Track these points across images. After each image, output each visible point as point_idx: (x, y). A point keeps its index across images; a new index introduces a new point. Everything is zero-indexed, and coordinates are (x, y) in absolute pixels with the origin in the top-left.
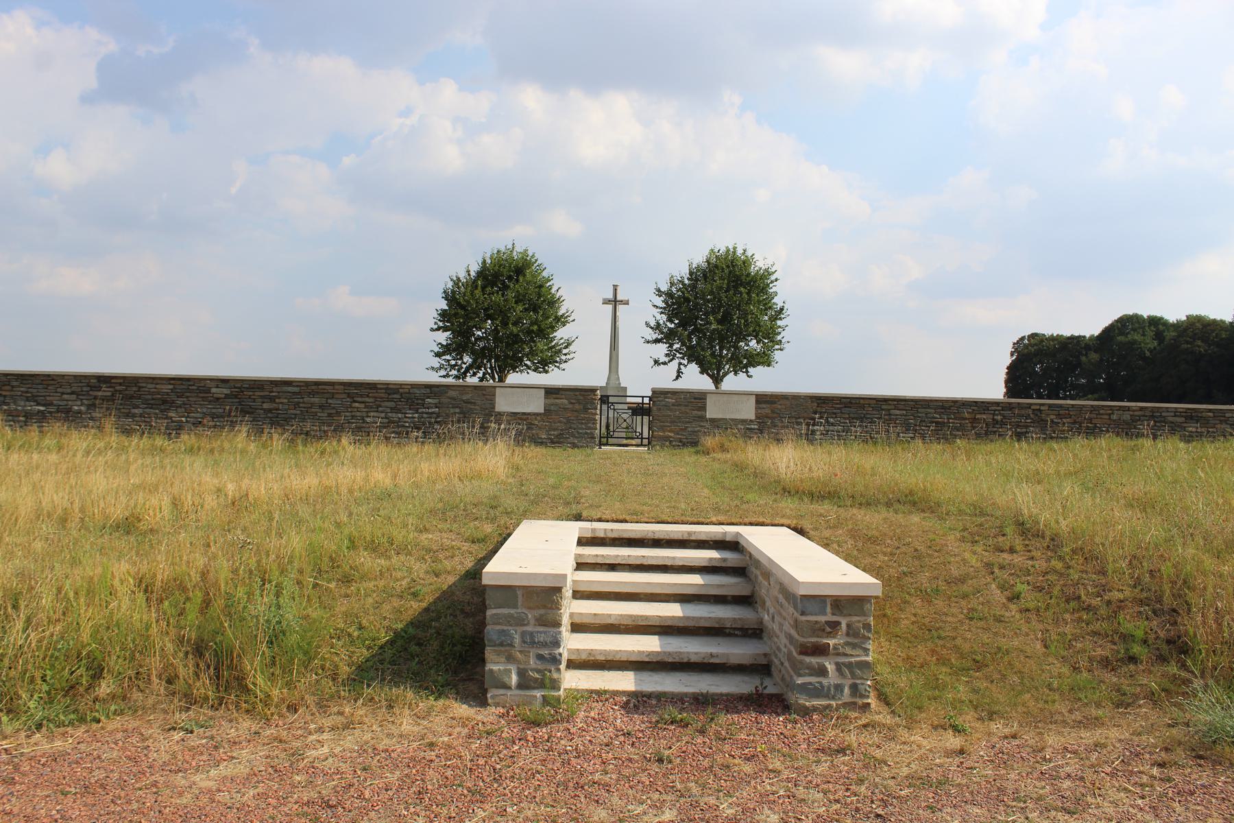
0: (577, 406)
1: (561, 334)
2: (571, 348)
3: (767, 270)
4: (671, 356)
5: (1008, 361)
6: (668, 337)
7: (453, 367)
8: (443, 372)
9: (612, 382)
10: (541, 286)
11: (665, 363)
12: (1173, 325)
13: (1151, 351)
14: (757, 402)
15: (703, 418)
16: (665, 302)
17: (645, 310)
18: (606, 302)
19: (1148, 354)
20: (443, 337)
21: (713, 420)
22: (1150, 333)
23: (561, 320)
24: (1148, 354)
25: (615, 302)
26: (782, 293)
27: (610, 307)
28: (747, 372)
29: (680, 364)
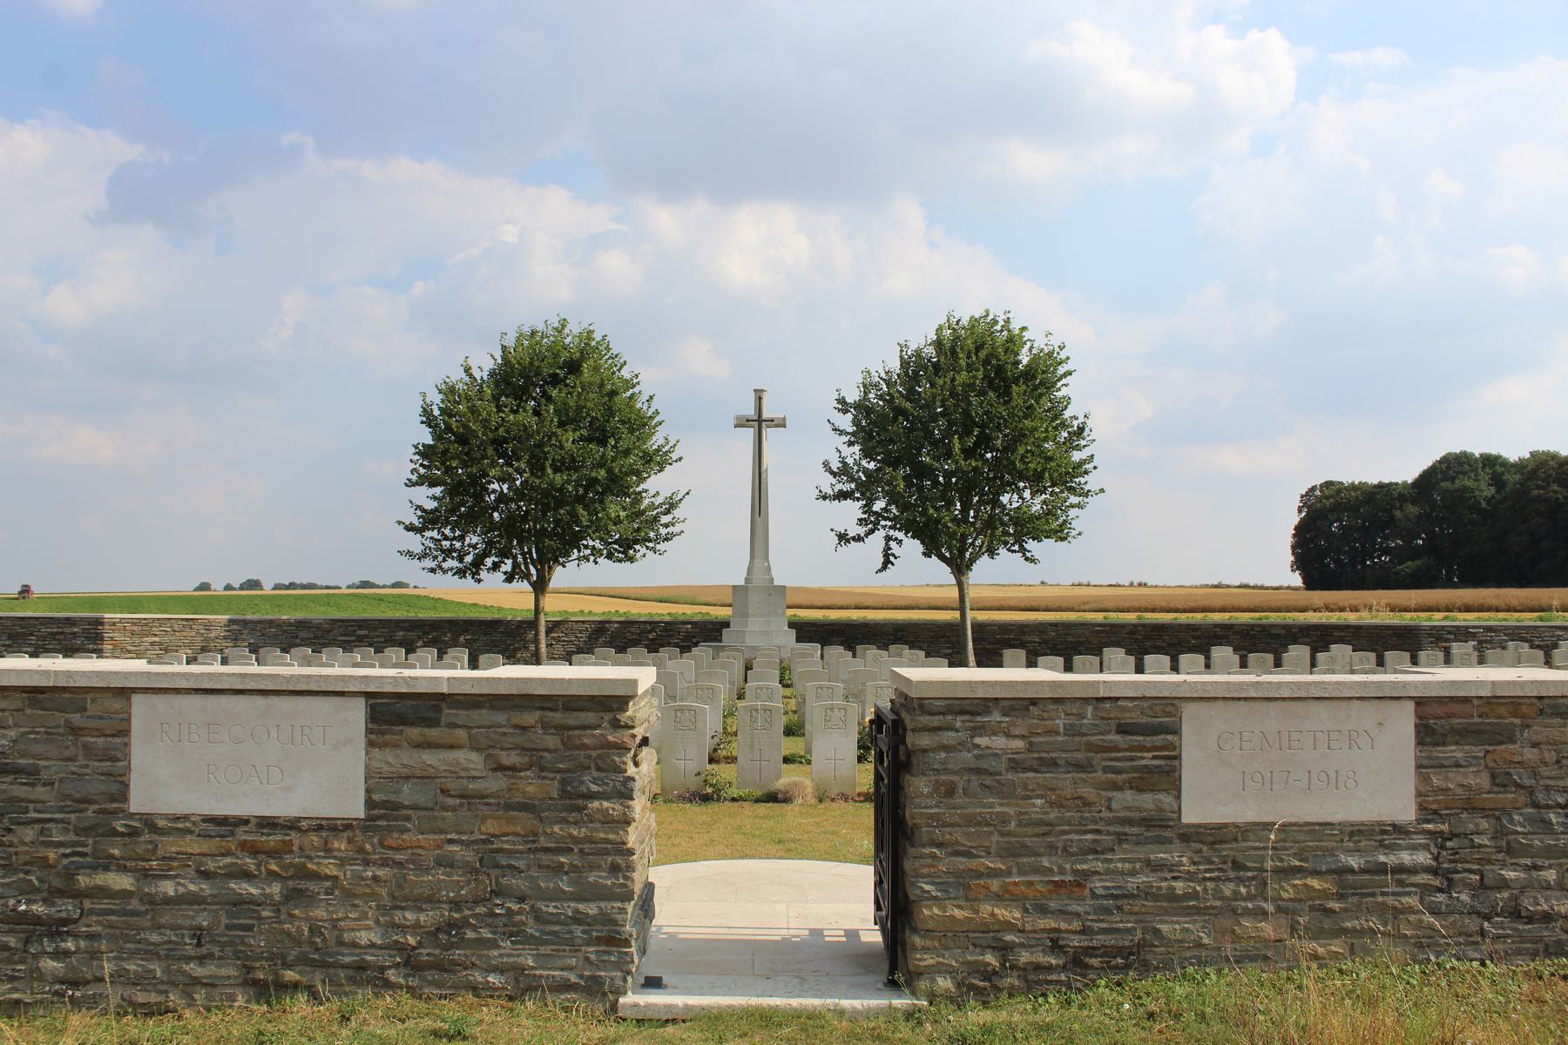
0: (531, 786)
1: (657, 486)
2: (676, 513)
3: (1050, 354)
4: (871, 521)
5: (1295, 519)
6: (865, 489)
7: (448, 553)
8: (429, 563)
9: (758, 577)
10: (613, 394)
11: (858, 539)
12: (1514, 465)
13: (1488, 502)
14: (1426, 734)
15: (1160, 826)
16: (856, 422)
17: (815, 446)
18: (742, 423)
19: (1484, 504)
20: (426, 497)
21: (1212, 836)
22: (1485, 477)
23: (657, 460)
24: (1484, 504)
25: (758, 423)
26: (1080, 396)
27: (749, 433)
28: (1023, 550)
29: (888, 538)
